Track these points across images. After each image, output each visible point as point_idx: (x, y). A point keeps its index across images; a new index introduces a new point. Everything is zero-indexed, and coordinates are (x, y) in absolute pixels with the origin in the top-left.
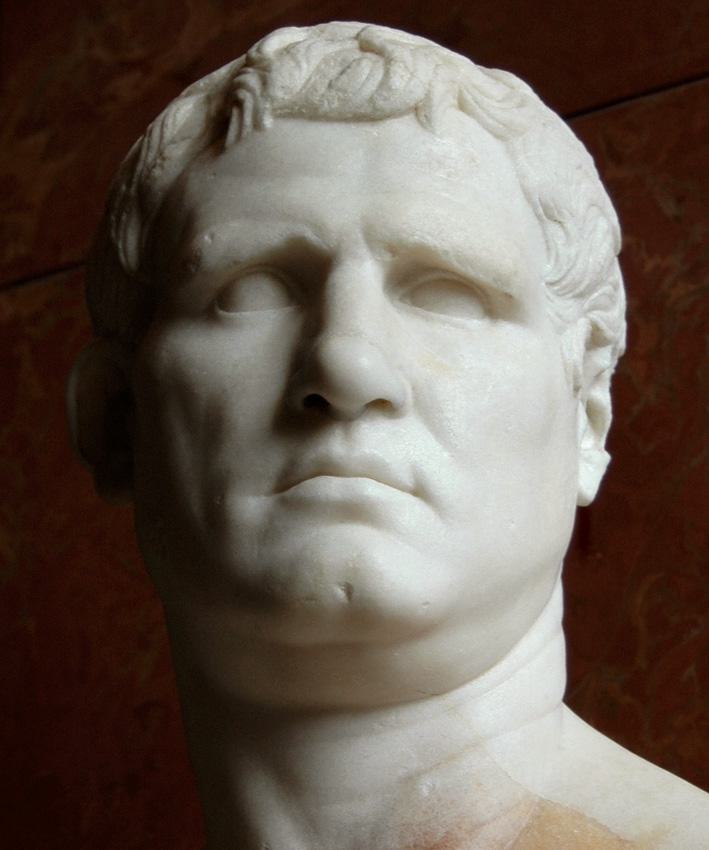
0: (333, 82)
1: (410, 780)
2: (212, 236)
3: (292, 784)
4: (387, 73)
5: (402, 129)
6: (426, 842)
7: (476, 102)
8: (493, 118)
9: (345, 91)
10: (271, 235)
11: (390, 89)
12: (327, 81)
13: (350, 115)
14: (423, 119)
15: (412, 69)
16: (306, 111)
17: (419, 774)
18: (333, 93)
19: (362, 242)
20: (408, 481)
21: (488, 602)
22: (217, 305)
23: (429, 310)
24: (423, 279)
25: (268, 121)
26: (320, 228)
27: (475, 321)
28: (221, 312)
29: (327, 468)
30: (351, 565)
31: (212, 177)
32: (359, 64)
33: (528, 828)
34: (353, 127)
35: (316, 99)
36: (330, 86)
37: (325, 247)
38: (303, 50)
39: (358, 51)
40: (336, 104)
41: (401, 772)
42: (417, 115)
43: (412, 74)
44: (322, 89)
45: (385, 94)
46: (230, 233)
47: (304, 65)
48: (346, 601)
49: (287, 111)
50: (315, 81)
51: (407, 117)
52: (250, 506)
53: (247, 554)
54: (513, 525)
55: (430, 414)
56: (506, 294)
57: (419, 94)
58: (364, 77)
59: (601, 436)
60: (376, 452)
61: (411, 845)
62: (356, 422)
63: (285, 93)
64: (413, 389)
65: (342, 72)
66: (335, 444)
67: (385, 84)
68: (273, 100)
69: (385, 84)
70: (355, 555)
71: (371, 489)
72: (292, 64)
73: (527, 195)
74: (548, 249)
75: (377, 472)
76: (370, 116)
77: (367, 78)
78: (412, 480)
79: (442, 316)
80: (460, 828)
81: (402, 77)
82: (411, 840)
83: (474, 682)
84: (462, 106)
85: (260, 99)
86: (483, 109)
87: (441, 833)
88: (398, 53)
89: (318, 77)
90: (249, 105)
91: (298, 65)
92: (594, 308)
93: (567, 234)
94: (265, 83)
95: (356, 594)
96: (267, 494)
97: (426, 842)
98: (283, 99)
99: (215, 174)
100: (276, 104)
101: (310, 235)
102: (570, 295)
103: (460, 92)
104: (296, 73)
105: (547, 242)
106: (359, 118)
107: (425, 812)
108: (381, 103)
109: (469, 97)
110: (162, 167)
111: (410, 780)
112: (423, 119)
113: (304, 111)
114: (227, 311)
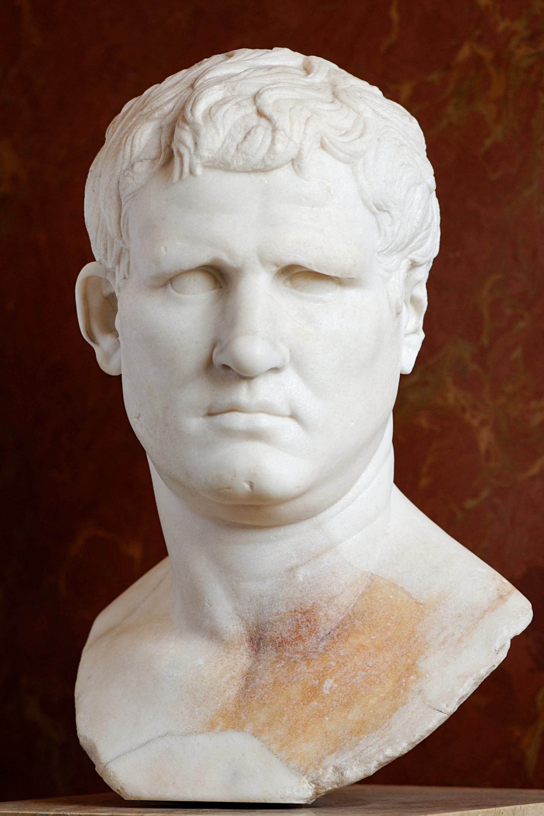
1: (292, 570)
2: (166, 249)
5: (284, 176)
6: (301, 609)
8: (341, 151)
9: (247, 154)
10: (204, 256)
11: (275, 153)
12: (235, 145)
13: (250, 170)
14: (296, 167)
16: (221, 165)
17: (297, 566)
18: (240, 155)
20: (288, 412)
21: (341, 470)
25: (199, 171)
27: (330, 294)
28: (172, 291)
30: (253, 472)
33: (363, 594)
34: (252, 175)
35: (228, 158)
37: (235, 266)
39: (255, 116)
40: (241, 163)
42: (293, 164)
43: (289, 139)
44: (233, 151)
45: (272, 156)
47: (221, 131)
48: (250, 490)
49: (211, 164)
51: (286, 166)
54: (353, 424)
55: (298, 362)
56: (349, 278)
57: (293, 152)
58: (259, 143)
59: (420, 316)
60: (267, 399)
61: (293, 610)
63: (210, 153)
64: (290, 351)
65: (245, 138)
66: (242, 394)
67: (271, 148)
68: (201, 158)
69: (271, 148)
70: (254, 465)
71: (264, 421)
72: (214, 131)
73: (365, 203)
75: (267, 410)
76: (264, 169)
77: (261, 144)
80: (321, 600)
82: (292, 607)
83: (331, 508)
84: (323, 146)
85: (193, 155)
87: (310, 603)
88: (283, 121)
89: (230, 140)
90: (186, 159)
92: (410, 253)
93: (392, 217)
95: (255, 487)
96: (203, 417)
97: (301, 609)
98: (208, 157)
102: (395, 252)
103: (322, 137)
105: (379, 225)
106: (255, 171)
107: (301, 591)
108: (269, 162)
109: (327, 141)
112: (296, 167)
113: (221, 165)
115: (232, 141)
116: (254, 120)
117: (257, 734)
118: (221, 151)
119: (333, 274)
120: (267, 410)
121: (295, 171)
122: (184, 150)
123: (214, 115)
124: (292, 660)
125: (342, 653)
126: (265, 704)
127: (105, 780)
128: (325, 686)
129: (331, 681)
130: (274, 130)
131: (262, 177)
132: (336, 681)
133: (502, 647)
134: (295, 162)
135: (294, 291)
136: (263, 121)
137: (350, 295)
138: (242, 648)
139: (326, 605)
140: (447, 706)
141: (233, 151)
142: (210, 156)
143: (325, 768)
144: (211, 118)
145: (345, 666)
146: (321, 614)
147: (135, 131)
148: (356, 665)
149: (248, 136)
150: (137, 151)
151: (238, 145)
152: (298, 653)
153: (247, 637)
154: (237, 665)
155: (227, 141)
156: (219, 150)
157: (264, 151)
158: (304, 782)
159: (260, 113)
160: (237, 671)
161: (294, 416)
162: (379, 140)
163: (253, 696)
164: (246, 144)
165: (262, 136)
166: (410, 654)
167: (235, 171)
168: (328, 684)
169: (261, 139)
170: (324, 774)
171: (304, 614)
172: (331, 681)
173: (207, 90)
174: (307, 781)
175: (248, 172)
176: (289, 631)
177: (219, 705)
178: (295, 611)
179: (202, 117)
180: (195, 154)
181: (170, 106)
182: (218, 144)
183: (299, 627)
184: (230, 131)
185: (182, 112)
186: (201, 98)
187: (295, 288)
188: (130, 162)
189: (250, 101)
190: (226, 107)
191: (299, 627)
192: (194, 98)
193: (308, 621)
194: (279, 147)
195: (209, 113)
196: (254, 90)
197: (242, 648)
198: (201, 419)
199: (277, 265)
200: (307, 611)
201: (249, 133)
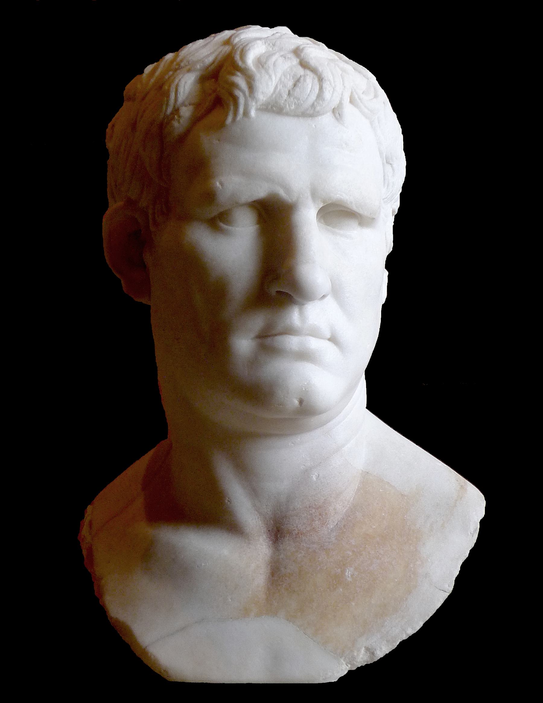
0: (291, 92)
1: (307, 472)
2: (221, 184)
3: (244, 470)
4: (321, 88)
5: (326, 120)
7: (360, 99)
8: (365, 107)
9: (299, 99)
11: (323, 100)
15: (333, 85)
16: (274, 108)
18: (292, 99)
19: (310, 197)
20: (329, 336)
22: (219, 221)
23: (333, 227)
24: (336, 213)
26: (288, 190)
28: (222, 224)
29: (290, 331)
31: (217, 141)
32: (305, 80)
34: (301, 120)
35: (282, 102)
36: (289, 94)
37: (290, 201)
38: (272, 67)
39: (300, 67)
41: (302, 467)
44: (285, 96)
46: (234, 183)
47: (274, 78)
48: (299, 406)
50: (280, 90)
52: (243, 344)
53: (242, 370)
55: (337, 291)
58: (309, 90)
61: (308, 506)
62: (306, 306)
65: (295, 85)
66: (294, 316)
69: (320, 95)
71: (314, 344)
72: (267, 77)
73: (381, 153)
74: (384, 180)
75: (315, 333)
76: (309, 113)
78: (330, 334)
79: (342, 232)
81: (329, 91)
86: (357, 94)
88: (327, 74)
90: (242, 101)
91: (270, 76)
94: (251, 87)
95: (304, 403)
96: (252, 339)
99: (219, 140)
100: (259, 103)
101: (282, 193)
103: (352, 93)
104: (270, 83)
110: (179, 122)
111: (307, 472)
112: (337, 115)
114: (224, 223)
115: (283, 87)
116: (301, 71)
117: (291, 618)
118: (274, 96)
119: (361, 212)
120: (315, 333)
121: (337, 119)
122: (237, 93)
123: (265, 63)
124: (310, 550)
125: (353, 542)
126: (294, 591)
127: (132, 648)
128: (347, 574)
129: (352, 569)
130: (321, 79)
131: (309, 121)
132: (356, 569)
133: (475, 530)
134: (337, 112)
135: (328, 227)
136: (308, 72)
137: (366, 233)
138: (261, 539)
139: (334, 500)
140: (449, 586)
141: (286, 96)
142: (264, 99)
143: (359, 650)
144: (263, 67)
145: (361, 555)
146: (331, 508)
147: (177, 80)
148: (369, 553)
149: (298, 83)
150: (181, 97)
151: (289, 91)
152: (313, 543)
153: (265, 529)
154: (259, 555)
155: (279, 87)
156: (272, 95)
157: (313, 97)
158: (342, 664)
159: (304, 65)
160: (261, 560)
161: (333, 340)
162: (384, 103)
163: (281, 583)
164: (297, 90)
165: (310, 81)
166: (410, 542)
167: (287, 114)
168: (348, 573)
169: (310, 87)
170: (358, 655)
171: (317, 509)
172: (352, 569)
173: (253, 44)
174: (344, 663)
175: (297, 116)
176: (304, 524)
177: (250, 593)
178: (310, 507)
179: (253, 65)
180: (250, 96)
181: (211, 59)
182: (271, 89)
183: (313, 520)
184: (280, 79)
185: (187, 103)
186: (249, 49)
187: (328, 226)
188: (174, 106)
189: (291, 56)
190: (274, 59)
191: (313, 520)
192: (238, 53)
193: (320, 515)
194: (327, 95)
195: (261, 62)
196: (293, 47)
197: (261, 539)
198: (250, 340)
199: (324, 202)
200: (320, 507)
201: (298, 80)
